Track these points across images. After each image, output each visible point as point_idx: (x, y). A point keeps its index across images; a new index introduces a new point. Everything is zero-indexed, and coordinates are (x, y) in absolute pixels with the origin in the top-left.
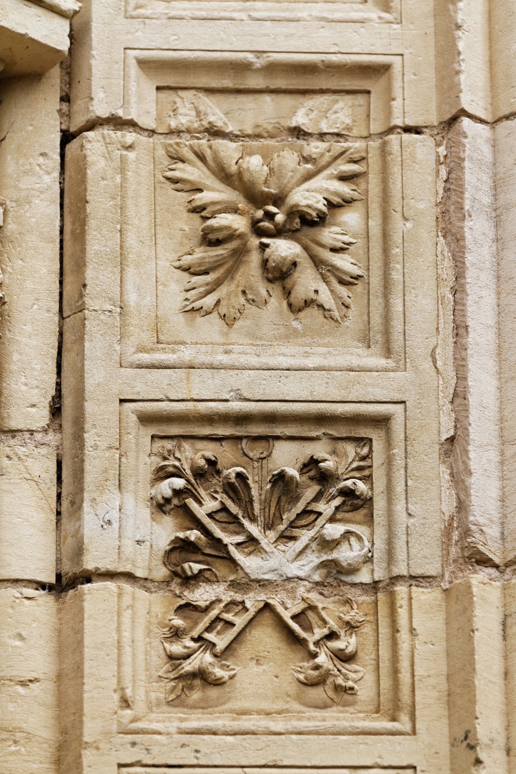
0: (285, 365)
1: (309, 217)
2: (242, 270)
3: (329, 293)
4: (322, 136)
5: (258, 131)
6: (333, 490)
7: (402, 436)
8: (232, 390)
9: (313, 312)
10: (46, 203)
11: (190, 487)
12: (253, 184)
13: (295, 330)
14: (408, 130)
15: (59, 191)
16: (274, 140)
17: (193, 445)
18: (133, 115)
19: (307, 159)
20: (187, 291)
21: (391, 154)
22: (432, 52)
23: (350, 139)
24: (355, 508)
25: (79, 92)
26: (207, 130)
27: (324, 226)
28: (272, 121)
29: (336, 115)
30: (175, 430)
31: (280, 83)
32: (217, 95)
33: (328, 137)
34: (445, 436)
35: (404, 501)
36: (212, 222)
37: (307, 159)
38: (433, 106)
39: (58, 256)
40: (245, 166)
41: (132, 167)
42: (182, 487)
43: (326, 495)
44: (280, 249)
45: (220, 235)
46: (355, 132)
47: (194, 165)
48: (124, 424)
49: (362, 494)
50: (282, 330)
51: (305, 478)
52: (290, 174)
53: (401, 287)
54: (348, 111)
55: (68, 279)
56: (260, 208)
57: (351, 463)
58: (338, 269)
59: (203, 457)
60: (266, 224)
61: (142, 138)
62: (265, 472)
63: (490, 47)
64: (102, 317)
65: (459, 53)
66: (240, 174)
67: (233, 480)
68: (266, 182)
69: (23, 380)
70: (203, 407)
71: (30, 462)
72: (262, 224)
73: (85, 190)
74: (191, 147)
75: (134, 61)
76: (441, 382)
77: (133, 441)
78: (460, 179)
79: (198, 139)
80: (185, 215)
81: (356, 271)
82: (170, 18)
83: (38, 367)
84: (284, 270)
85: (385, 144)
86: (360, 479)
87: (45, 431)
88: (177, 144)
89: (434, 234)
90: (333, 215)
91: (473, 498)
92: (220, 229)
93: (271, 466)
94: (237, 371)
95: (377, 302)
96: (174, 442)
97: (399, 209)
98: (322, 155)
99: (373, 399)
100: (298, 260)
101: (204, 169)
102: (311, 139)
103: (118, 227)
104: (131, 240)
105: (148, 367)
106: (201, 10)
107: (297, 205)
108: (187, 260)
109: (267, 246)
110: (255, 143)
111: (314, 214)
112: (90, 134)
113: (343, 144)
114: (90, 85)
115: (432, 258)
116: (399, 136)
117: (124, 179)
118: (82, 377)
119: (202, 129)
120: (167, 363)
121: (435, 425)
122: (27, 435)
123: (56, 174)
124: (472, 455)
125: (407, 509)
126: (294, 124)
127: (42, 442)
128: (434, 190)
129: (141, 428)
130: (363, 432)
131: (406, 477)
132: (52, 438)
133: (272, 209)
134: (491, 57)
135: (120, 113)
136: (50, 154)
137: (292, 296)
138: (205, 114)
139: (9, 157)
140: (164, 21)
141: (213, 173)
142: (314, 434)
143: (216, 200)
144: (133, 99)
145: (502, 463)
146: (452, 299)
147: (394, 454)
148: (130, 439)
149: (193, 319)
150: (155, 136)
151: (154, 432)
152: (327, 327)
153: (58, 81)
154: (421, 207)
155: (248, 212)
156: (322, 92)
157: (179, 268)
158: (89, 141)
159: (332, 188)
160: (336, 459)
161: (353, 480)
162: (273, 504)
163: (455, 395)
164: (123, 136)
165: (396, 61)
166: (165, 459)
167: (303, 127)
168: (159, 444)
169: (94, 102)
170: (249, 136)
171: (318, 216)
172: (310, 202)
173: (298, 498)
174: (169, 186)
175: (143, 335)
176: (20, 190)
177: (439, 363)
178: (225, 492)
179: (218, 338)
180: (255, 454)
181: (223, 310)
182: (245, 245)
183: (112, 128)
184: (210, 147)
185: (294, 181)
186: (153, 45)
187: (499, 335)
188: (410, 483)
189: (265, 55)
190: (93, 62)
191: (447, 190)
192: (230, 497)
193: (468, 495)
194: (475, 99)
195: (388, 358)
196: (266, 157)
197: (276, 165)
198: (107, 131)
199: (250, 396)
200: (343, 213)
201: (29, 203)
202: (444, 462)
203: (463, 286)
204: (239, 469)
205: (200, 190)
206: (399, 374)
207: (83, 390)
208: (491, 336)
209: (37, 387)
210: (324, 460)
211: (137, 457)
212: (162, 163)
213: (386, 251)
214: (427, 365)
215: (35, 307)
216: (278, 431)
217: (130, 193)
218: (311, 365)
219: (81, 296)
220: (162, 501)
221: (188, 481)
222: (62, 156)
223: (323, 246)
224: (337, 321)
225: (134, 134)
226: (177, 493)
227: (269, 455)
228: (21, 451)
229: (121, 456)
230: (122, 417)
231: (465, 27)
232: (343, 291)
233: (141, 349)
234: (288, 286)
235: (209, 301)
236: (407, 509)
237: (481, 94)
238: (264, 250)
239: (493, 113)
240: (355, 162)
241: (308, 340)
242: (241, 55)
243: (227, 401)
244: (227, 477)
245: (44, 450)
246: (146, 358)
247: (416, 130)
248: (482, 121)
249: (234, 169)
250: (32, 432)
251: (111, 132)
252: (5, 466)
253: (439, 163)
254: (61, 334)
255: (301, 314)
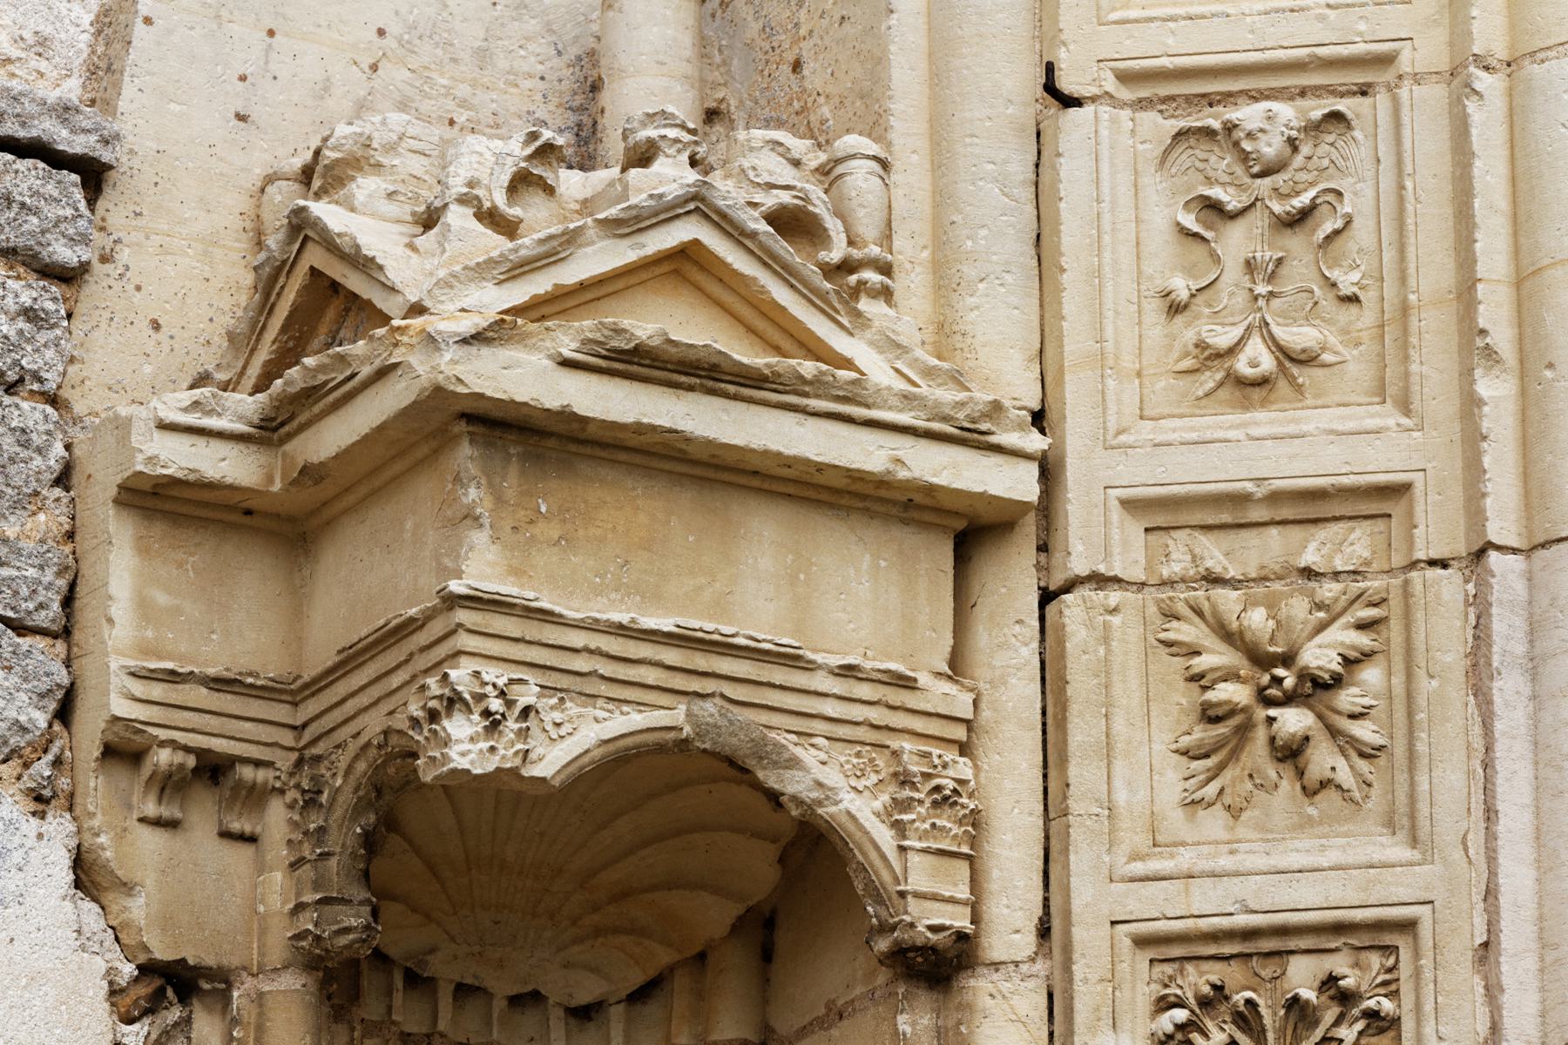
0: (1296, 867)
1: (1321, 681)
2: (1247, 749)
3: (1348, 769)
4: (1336, 575)
5: (1263, 573)
6: (1356, 1012)
7: (1431, 944)
8: (1236, 902)
9: (1331, 794)
10: (1024, 682)
11: (1194, 1018)
12: (1256, 644)
13: (1310, 817)
14: (1432, 563)
15: (1038, 665)
16: (1283, 582)
17: (1197, 966)
18: (1117, 571)
19: (1319, 606)
20: (1186, 779)
21: (1412, 596)
22: (1459, 464)
23: (1369, 575)
24: (1381, 1031)
25: (1056, 542)
26: (1204, 578)
27: (1340, 687)
28: (1280, 560)
29: (1352, 548)
30: (1177, 951)
31: (1287, 513)
32: (1216, 531)
33: (1343, 576)
34: (1479, 941)
35: (1434, 1022)
36: (1211, 696)
37: (1319, 606)
38: (1461, 532)
39: (1040, 745)
40: (1246, 623)
41: (1117, 634)
42: (1184, 1020)
43: (1348, 1017)
44: (1288, 725)
45: (1220, 712)
46: (1375, 566)
47: (1191, 623)
48: (1116, 951)
49: (1388, 1015)
50: (1296, 819)
51: (1323, 998)
52: (1300, 626)
53: (1426, 761)
54: (1366, 541)
55: (1052, 773)
56: (1267, 670)
57: (1375, 977)
58: (1357, 740)
59: (1208, 982)
60: (1273, 692)
61: (1129, 594)
62: (1279, 992)
63: (1524, 456)
64: (1088, 823)
65: (1485, 471)
66: (1241, 633)
67: (1242, 1008)
68: (1272, 640)
69: (1005, 901)
70: (1204, 924)
71: (1015, 1001)
72: (1269, 692)
73: (1065, 667)
74: (1187, 601)
75: (1116, 503)
76: (1474, 875)
77: (1128, 970)
78: (1488, 628)
79: (1195, 589)
80: (1182, 684)
81: (1378, 740)
82: (1155, 445)
83: (1021, 884)
84: (1294, 747)
85: (1406, 583)
86: (1386, 996)
87: (1033, 960)
88: (1170, 599)
89: (1463, 692)
90: (1350, 673)
91: (1505, 1020)
92: (1219, 704)
93: (1286, 986)
94: (1241, 878)
95: (1402, 778)
96: (1176, 965)
97: (1423, 664)
98: (1336, 600)
99: (1396, 900)
100: (1310, 733)
101: (1203, 626)
102: (1324, 579)
103: (1104, 710)
104: (1119, 725)
105: (1141, 880)
106: (1192, 429)
107: (1307, 668)
108: (1185, 741)
109: (1274, 719)
110: (1259, 590)
111: (1327, 676)
112: (1067, 597)
113: (1360, 584)
114: (1067, 535)
115: (1461, 722)
116: (1421, 573)
117: (1109, 651)
118: (1069, 896)
119: (1199, 577)
120: (1163, 873)
121: (1467, 927)
122: (1011, 967)
123: (1035, 645)
124: (1504, 968)
125: (1437, 1031)
126: (1303, 565)
127: (1029, 973)
128: (1463, 639)
129: (1137, 951)
130: (1388, 939)
131: (1436, 992)
132: (1040, 967)
133: (1280, 672)
134: (1525, 467)
135: (1102, 569)
136: (1027, 620)
137: (1306, 776)
138: (1202, 558)
139: (981, 628)
140: (1148, 449)
141: (1213, 630)
142: (1333, 945)
143: (1215, 666)
144: (1116, 550)
145: (1542, 970)
146: (1482, 774)
147: (1421, 966)
148: (1124, 968)
149: (1194, 814)
150: (1146, 588)
151: (1152, 956)
152: (1346, 812)
153: (1034, 528)
154: (1449, 659)
155: (1252, 678)
156: (1336, 519)
157: (1176, 751)
158: (1068, 607)
159: (1348, 641)
160: (1358, 972)
161: (1377, 998)
162: (1289, 1032)
163: (1488, 892)
164: (1106, 597)
165: (1417, 478)
166: (1166, 986)
167: (1314, 567)
168: (1159, 969)
169: (1072, 558)
170: (1253, 580)
171: (1332, 678)
172: (1321, 663)
173: (1316, 1023)
174: (1164, 651)
175: (1137, 839)
176: (994, 668)
177: (1471, 852)
178: (1234, 1022)
179: (1223, 835)
180: (1266, 973)
181: (1227, 800)
182: (1250, 718)
183: (1095, 586)
184: (1208, 599)
185: (1304, 635)
186: (1138, 480)
187: (1537, 815)
188: (1440, 999)
189: (1267, 482)
190: (1069, 507)
191: (1476, 637)
192: (1239, 1028)
193: (1501, 1016)
194: (1505, 525)
195: (1414, 848)
196: (1272, 605)
197: (1284, 616)
198: (1084, 592)
199: (1257, 908)
200: (1362, 670)
201: (1005, 683)
202: (1479, 972)
203: (1492, 760)
204: (1249, 994)
205: (1198, 653)
206: (1425, 867)
207: (1070, 913)
208: (1527, 817)
209: (1021, 908)
210: (1344, 977)
211: (1133, 988)
212: (1153, 623)
213: (1410, 714)
214: (1458, 854)
215: (1016, 811)
216: (1292, 944)
217: (1116, 667)
218: (1326, 865)
219: (1065, 798)
220: (1163, 1038)
221: (1192, 1011)
222: (1042, 618)
223: (1339, 713)
224: (1358, 803)
225: (1118, 594)
226: (1180, 1027)
227: (1284, 974)
228: (1006, 987)
229: (1114, 989)
230: (1116, 942)
231: (1492, 437)
232: (1363, 765)
233: (1135, 857)
234: (1301, 765)
235: (1211, 790)
236: (1437, 1031)
237: (1513, 517)
238: (1271, 724)
239: (1529, 537)
240: (1375, 605)
241: (1326, 829)
242: (1238, 485)
243: (1231, 914)
244: (1235, 1005)
245: (1031, 984)
246: (1139, 868)
247: (1444, 564)
248: (1514, 551)
249: (1235, 625)
250: (1017, 964)
251: (1092, 593)
252: (988, 1006)
253: (1467, 604)
254: (1047, 838)
255: (1318, 798)
